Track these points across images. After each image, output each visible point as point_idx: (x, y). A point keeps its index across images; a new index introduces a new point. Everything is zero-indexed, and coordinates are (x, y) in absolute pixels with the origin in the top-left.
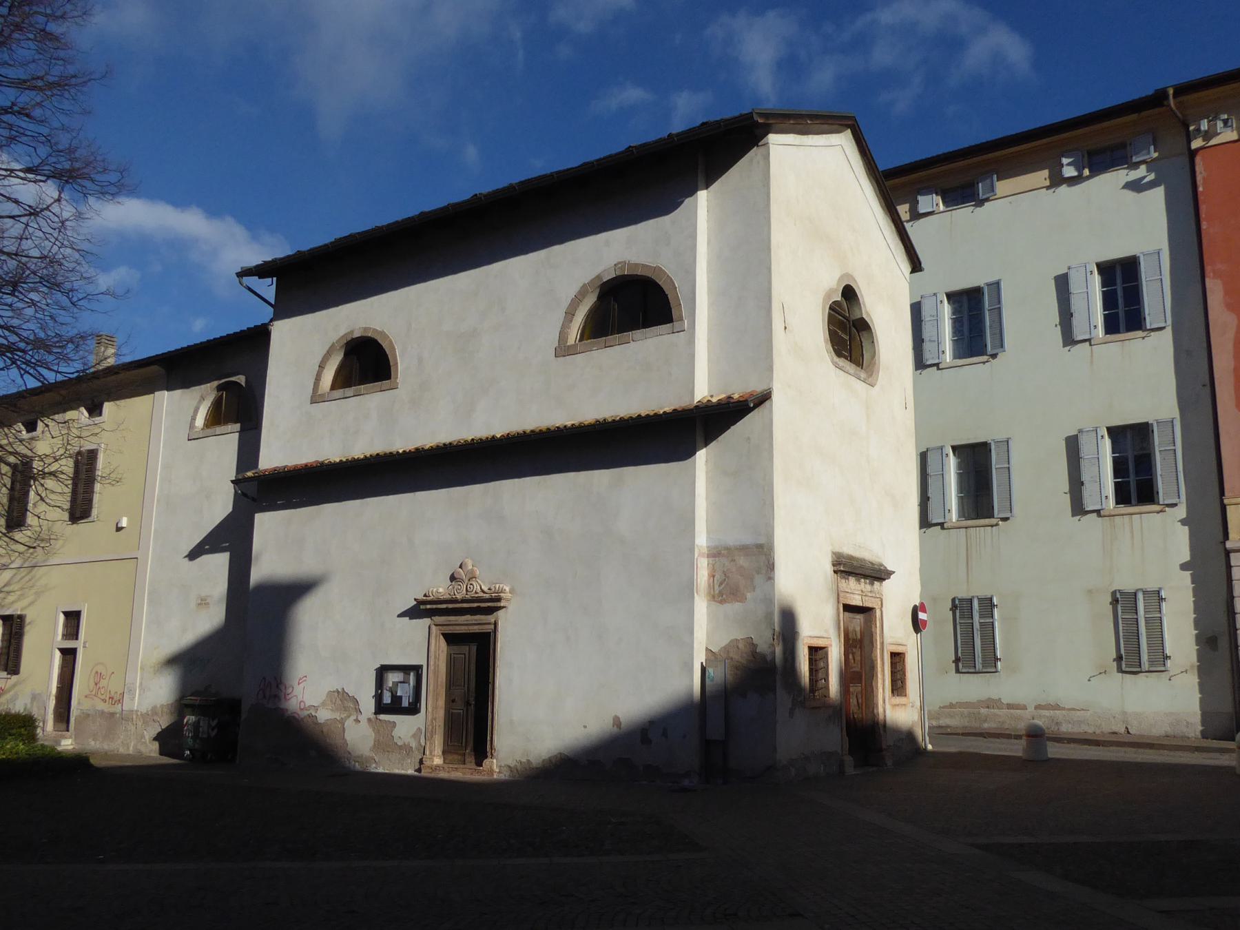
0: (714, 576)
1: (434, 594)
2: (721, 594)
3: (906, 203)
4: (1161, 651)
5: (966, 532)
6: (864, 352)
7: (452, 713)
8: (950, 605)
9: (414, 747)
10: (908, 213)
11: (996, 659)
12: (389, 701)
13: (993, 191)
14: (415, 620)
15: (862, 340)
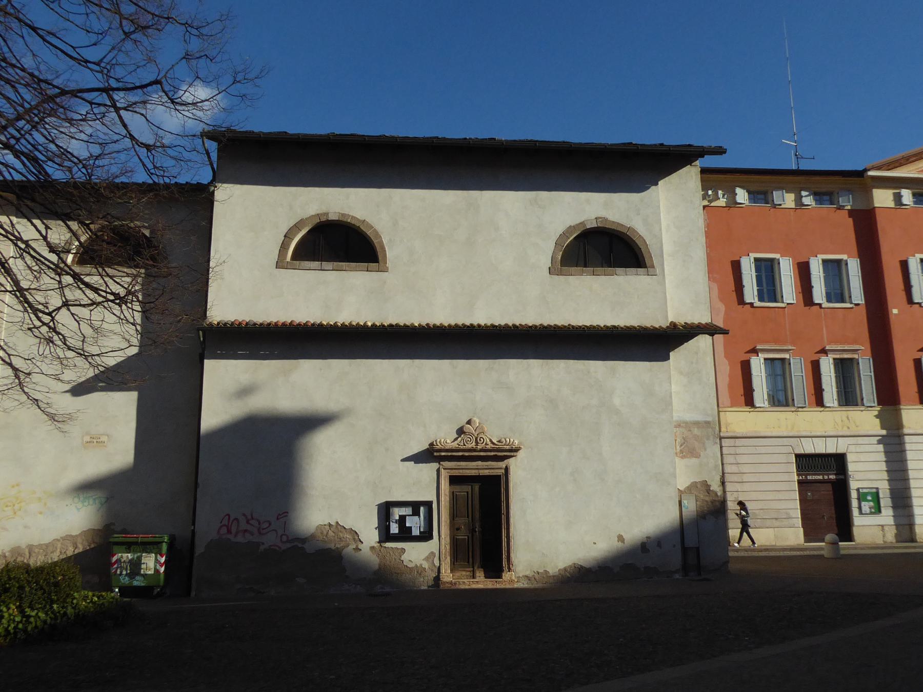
1: (443, 444)
2: (681, 452)
7: (456, 538)
9: (427, 568)
12: (397, 532)
14: (421, 464)
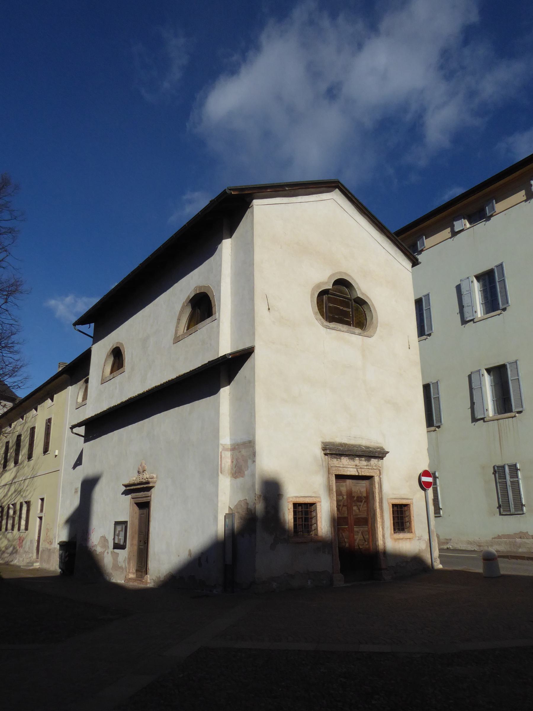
0: (233, 462)
3: (448, 228)
4: (507, 497)
5: (498, 423)
6: (367, 317)
8: (492, 471)
10: (450, 233)
11: (523, 505)
13: (494, 210)
15: (365, 310)
